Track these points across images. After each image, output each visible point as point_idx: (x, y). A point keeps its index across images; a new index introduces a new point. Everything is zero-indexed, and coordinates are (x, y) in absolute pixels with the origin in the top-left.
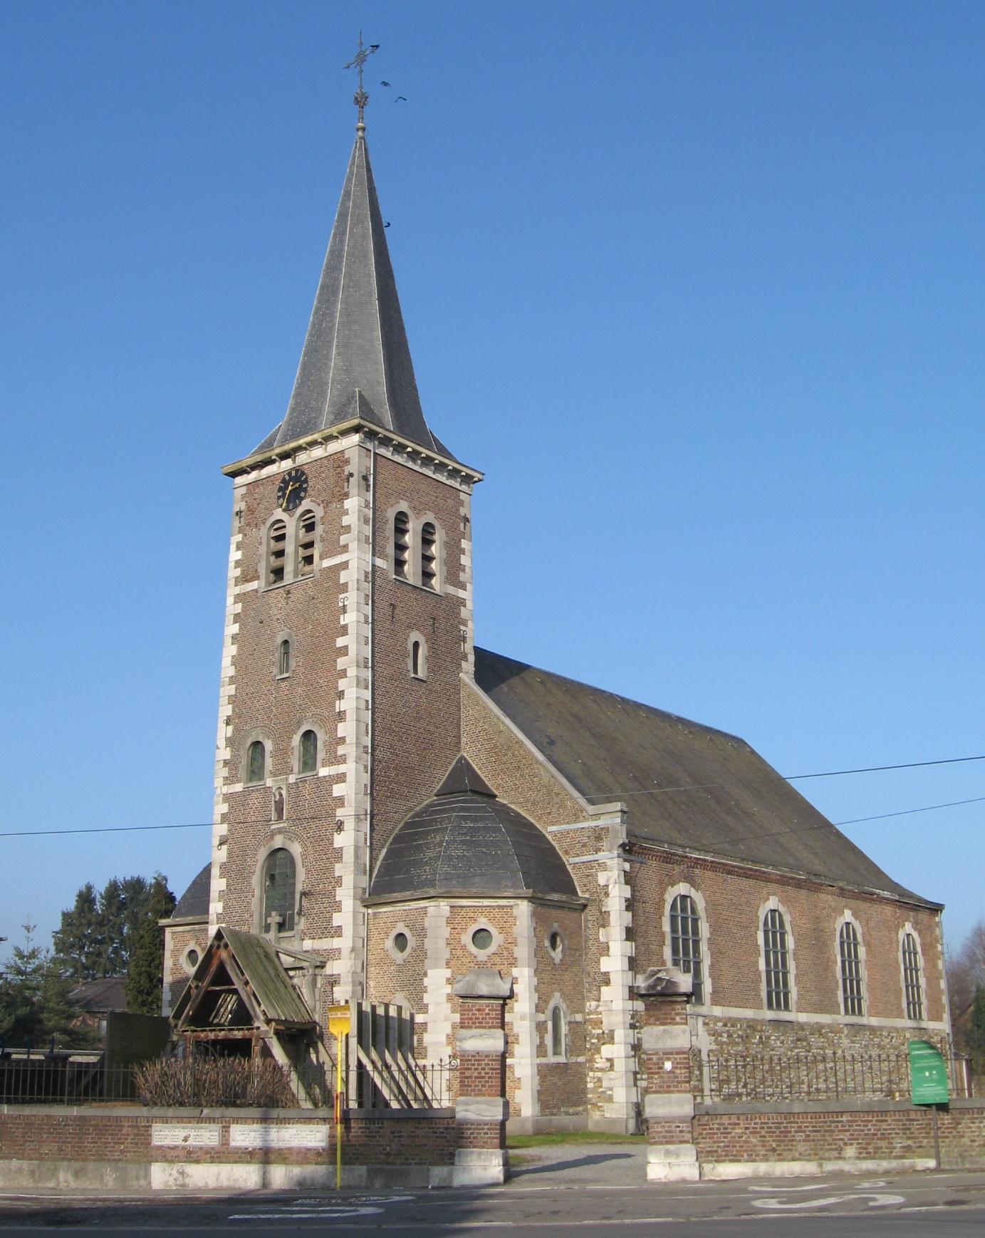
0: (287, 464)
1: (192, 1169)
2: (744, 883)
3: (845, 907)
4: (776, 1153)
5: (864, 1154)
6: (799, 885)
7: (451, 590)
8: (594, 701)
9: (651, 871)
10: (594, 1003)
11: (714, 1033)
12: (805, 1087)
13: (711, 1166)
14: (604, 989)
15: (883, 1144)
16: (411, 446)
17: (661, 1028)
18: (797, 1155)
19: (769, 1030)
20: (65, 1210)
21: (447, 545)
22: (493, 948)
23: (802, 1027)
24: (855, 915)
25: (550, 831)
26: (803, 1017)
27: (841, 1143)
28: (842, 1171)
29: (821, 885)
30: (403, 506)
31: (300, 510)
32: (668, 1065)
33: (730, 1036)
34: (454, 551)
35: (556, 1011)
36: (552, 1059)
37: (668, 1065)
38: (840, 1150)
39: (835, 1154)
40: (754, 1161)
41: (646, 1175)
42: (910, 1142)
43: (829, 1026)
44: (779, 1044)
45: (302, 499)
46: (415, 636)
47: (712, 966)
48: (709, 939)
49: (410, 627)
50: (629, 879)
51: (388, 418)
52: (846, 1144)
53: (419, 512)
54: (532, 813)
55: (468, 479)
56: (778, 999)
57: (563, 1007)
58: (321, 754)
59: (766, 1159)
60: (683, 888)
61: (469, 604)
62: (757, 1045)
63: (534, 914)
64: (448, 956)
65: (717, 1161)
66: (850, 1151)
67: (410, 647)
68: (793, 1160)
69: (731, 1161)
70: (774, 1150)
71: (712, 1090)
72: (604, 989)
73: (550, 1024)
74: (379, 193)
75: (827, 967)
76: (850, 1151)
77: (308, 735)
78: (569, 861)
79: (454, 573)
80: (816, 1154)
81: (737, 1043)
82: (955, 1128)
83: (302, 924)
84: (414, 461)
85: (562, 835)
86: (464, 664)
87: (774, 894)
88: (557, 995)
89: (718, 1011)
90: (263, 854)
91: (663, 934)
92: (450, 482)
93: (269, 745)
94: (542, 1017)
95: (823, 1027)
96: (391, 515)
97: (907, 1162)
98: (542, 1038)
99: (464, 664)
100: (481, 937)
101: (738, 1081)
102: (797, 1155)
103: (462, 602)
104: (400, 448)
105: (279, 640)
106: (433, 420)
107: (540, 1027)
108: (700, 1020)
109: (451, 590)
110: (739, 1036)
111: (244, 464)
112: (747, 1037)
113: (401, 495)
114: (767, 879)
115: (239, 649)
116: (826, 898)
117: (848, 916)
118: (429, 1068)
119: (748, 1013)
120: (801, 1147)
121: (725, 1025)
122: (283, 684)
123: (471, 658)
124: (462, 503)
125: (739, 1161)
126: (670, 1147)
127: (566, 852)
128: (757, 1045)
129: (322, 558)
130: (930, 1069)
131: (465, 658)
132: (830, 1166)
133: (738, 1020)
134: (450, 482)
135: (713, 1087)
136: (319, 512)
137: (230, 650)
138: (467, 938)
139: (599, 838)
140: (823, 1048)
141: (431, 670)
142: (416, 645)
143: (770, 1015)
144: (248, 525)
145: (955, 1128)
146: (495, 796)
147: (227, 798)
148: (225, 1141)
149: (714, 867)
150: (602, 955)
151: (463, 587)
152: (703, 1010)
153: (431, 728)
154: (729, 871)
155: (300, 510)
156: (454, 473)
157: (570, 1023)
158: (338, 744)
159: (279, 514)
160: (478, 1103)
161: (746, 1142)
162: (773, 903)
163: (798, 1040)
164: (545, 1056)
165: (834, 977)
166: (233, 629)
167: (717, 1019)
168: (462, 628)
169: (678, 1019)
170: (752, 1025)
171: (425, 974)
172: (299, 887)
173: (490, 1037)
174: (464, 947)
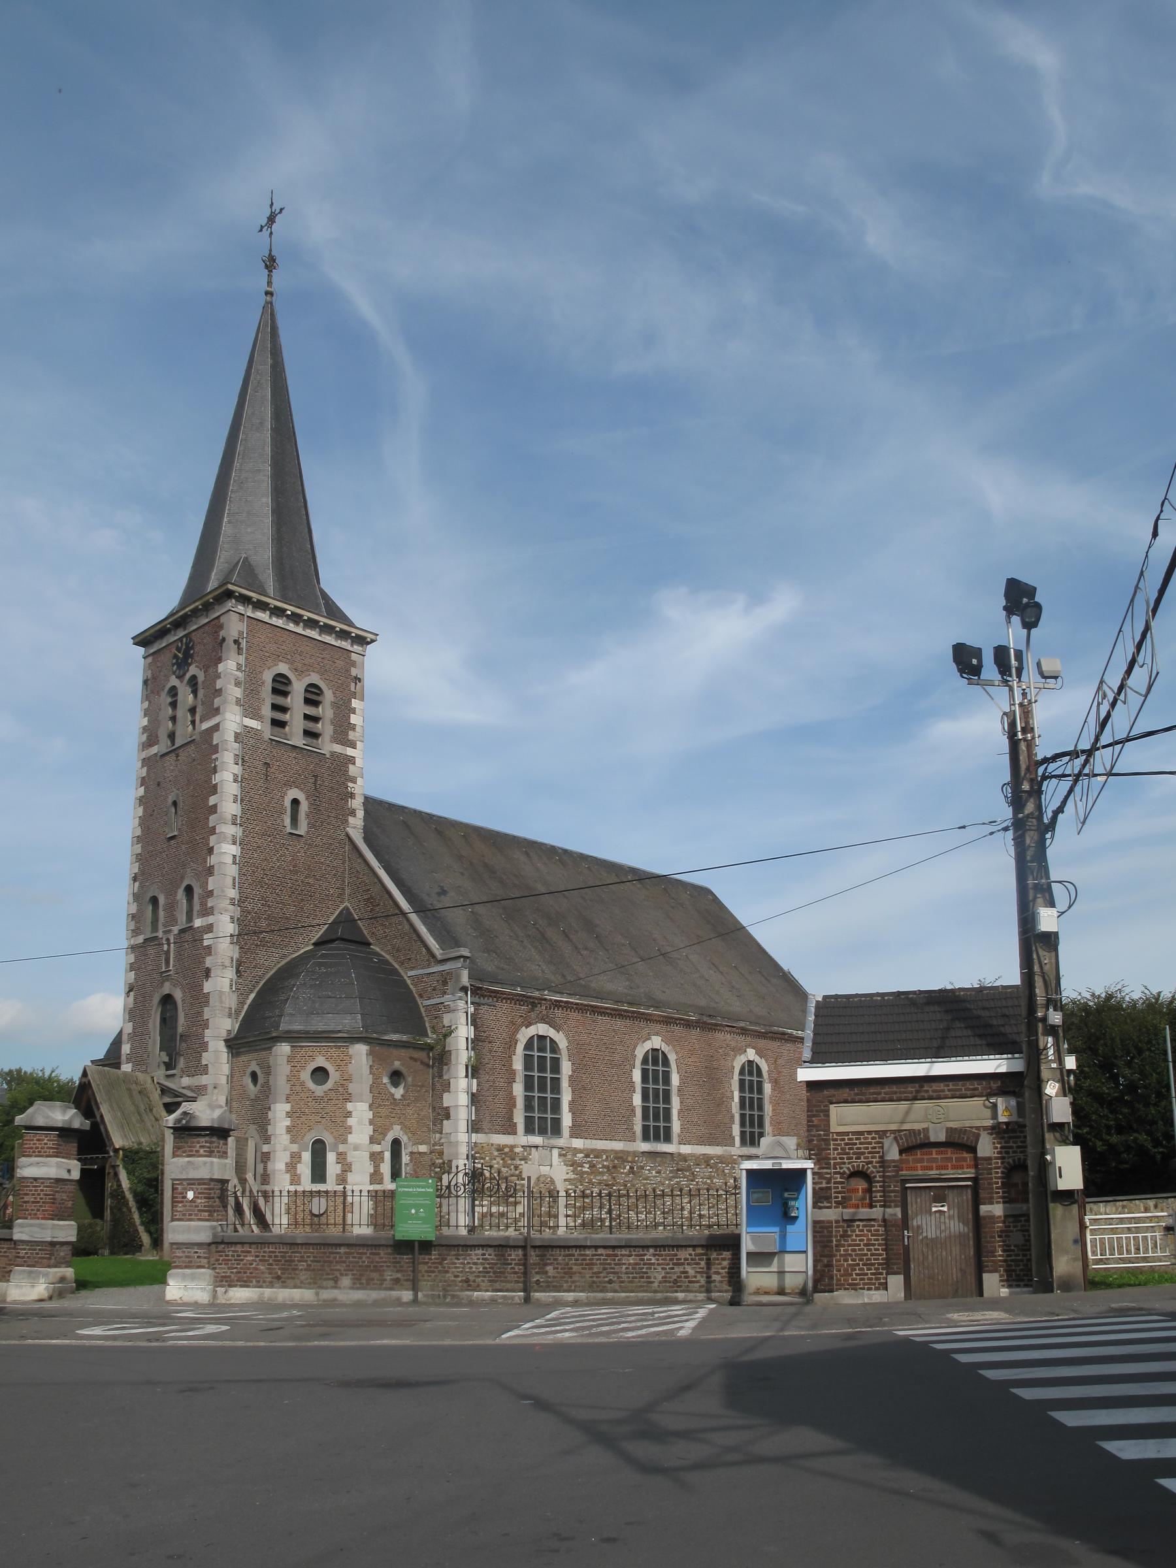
0: (181, 633)
2: (618, 1024)
3: (749, 1046)
4: (279, 1280)
5: (358, 1284)
6: (688, 1024)
7: (338, 748)
8: (527, 854)
9: (499, 1015)
10: (438, 1135)
11: (573, 1164)
12: (686, 1213)
13: (223, 1289)
14: (445, 1122)
15: (375, 1275)
16: (290, 609)
17: (187, 1159)
18: (298, 1282)
19: (643, 1161)
21: (334, 705)
22: (329, 1084)
23: (684, 1158)
24: (759, 1053)
25: (408, 975)
26: (686, 1149)
27: (337, 1274)
28: (335, 1300)
29: (716, 1025)
30: (283, 668)
31: (188, 676)
32: (190, 1195)
33: (592, 1166)
34: (344, 710)
35: (396, 1143)
36: (306, 1184)
37: (190, 1195)
38: (336, 1280)
39: (331, 1283)
40: (261, 1287)
41: (164, 1295)
42: (399, 1275)
43: (719, 1157)
44: (654, 1177)
45: (190, 664)
46: (294, 793)
47: (572, 1103)
48: (570, 1077)
49: (289, 784)
50: (475, 1021)
51: (270, 585)
52: (342, 1275)
53: (300, 673)
54: (396, 958)
55: (362, 641)
56: (657, 1130)
57: (404, 1139)
58: (197, 907)
59: (271, 1285)
60: (542, 1029)
61: (358, 762)
62: (627, 1174)
63: (370, 1053)
64: (288, 1092)
65: (230, 1286)
66: (346, 1281)
67: (287, 803)
68: (295, 1287)
69: (241, 1286)
70: (278, 1278)
71: (567, 1216)
72: (445, 1122)
73: (387, 1155)
75: (721, 1103)
76: (346, 1281)
78: (423, 1003)
79: (343, 731)
80: (315, 1283)
81: (602, 1174)
82: (441, 1263)
83: (182, 1063)
84: (297, 623)
85: (418, 979)
86: (351, 820)
87: (657, 1034)
88: (397, 1128)
89: (578, 1143)
90: (156, 999)
91: (513, 1073)
92: (338, 643)
94: (377, 1148)
95: (712, 1158)
96: (268, 677)
97: (395, 1293)
98: (265, 1169)
99: (351, 820)
100: (320, 1074)
101: (601, 1208)
102: (298, 1282)
103: (352, 760)
104: (278, 612)
105: (170, 801)
106: (331, 581)
107: (376, 1158)
108: (555, 1152)
109: (338, 748)
110: (604, 1167)
111: (1130, 658)
112: (615, 1167)
113: (278, 657)
114: (648, 1018)
115: (145, 811)
116: (724, 1038)
117: (751, 1054)
118: (277, 1193)
119: (618, 1146)
120: (303, 1276)
121: (587, 1156)
122: (173, 842)
123: (360, 814)
124: (354, 664)
125: (248, 1286)
126: (188, 1271)
127: (421, 996)
128: (627, 1174)
129: (201, 722)
131: (353, 813)
132: (326, 1294)
133: (605, 1151)
134: (338, 643)
135: (569, 1213)
136: (201, 677)
138: (306, 1076)
139: (445, 983)
140: (710, 1178)
141: (311, 825)
143: (645, 1147)
144: (152, 692)
145: (441, 1263)
146: (370, 944)
149: (580, 1008)
150: (444, 1091)
151: (353, 745)
152: (561, 1142)
153: (311, 881)
154: (594, 1010)
155: (188, 676)
156: (343, 635)
157: (411, 1153)
158: (208, 897)
159: (174, 681)
160: (31, 1225)
161: (256, 1269)
162: (656, 1042)
163: (678, 1170)
164: (381, 1183)
165: (729, 1111)
167: (576, 1151)
168: (350, 784)
169: (202, 1151)
170: (621, 1156)
171: (269, 1108)
172: (180, 1030)
173: (45, 1164)
174: (302, 1084)
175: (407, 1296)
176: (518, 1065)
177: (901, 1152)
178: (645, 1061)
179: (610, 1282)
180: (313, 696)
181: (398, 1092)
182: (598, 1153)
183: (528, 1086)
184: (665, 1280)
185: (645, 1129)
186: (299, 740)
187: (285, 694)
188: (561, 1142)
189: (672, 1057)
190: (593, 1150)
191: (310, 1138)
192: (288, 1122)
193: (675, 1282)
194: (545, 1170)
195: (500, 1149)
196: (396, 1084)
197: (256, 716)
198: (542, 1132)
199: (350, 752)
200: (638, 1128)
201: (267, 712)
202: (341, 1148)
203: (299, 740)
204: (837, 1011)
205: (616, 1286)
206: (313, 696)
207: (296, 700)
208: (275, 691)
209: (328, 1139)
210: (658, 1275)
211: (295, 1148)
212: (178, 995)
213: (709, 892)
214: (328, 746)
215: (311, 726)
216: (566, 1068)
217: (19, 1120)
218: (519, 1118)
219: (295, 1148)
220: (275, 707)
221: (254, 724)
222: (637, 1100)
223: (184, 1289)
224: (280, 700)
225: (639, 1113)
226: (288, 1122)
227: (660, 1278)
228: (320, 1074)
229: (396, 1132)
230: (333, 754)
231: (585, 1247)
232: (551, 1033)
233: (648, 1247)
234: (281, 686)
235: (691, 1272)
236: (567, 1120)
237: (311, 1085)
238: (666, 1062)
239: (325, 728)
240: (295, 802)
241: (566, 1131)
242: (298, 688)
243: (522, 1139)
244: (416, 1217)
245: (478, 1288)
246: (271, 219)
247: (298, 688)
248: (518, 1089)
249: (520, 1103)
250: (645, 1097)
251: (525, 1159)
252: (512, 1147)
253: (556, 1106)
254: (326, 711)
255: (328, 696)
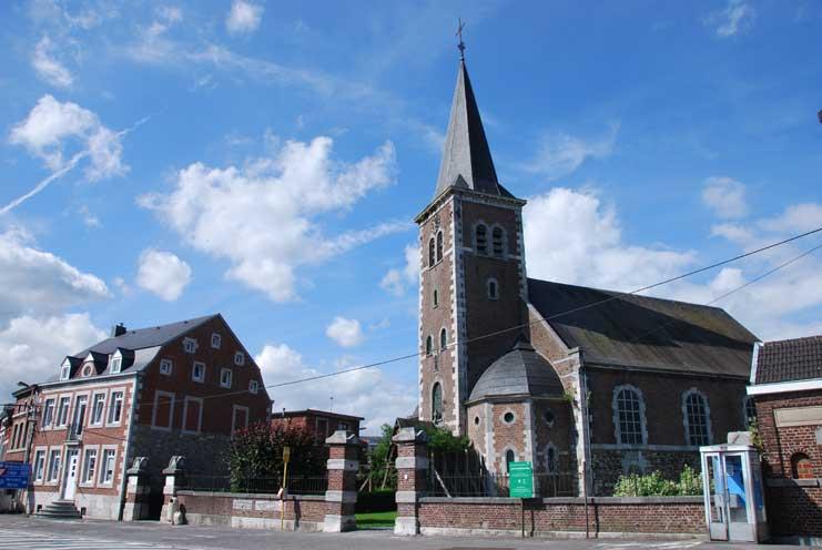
1: (244, 519)
7: (511, 256)
11: (650, 459)
20: (758, 531)
22: (513, 422)
25: (554, 363)
30: (482, 222)
33: (662, 460)
35: (551, 451)
36: (548, 473)
38: (481, 523)
53: (490, 223)
57: (555, 449)
60: (628, 387)
66: (485, 524)
73: (546, 457)
74: (472, 83)
77: (444, 331)
85: (559, 365)
93: (433, 338)
94: (540, 454)
96: (474, 227)
99: (521, 291)
108: (640, 453)
109: (511, 256)
119: (676, 448)
123: (526, 287)
130: (522, 478)
137: (421, 297)
138: (502, 418)
141: (501, 294)
142: (492, 285)
147: (422, 362)
148: (253, 507)
162: (694, 390)
166: (421, 288)
167: (653, 451)
174: (501, 423)
175: (519, 533)
176: (615, 407)
177: (394, 522)
178: (688, 401)
179: (638, 526)
180: (497, 234)
181: (551, 424)
182: (665, 453)
183: (622, 417)
184: (671, 526)
185: (692, 439)
186: (491, 254)
187: (500, 244)
188: (643, 447)
189: (705, 398)
190: (662, 451)
191: (505, 449)
192: (494, 442)
193: (679, 526)
194: (634, 463)
195: (608, 452)
196: (549, 421)
197: (470, 246)
198: (632, 442)
199: (518, 258)
200: (688, 437)
201: (475, 243)
202: (522, 454)
203: (491, 254)
204: (771, 351)
205: (642, 529)
206: (497, 234)
207: (489, 236)
208: (478, 233)
209: (515, 450)
210: (668, 521)
211: (498, 455)
212: (441, 382)
213: (722, 310)
214: (507, 256)
215: (498, 248)
216: (642, 406)
217: (328, 440)
218: (618, 435)
219: (498, 455)
220: (479, 241)
221: (469, 250)
222: (686, 422)
223: (404, 526)
224: (481, 237)
225: (688, 430)
226: (494, 442)
227: (668, 524)
228: (509, 417)
229: (550, 445)
230: (510, 259)
231: (620, 504)
232: (633, 388)
233: (659, 504)
234: (481, 231)
235: (689, 520)
236: (645, 435)
237: (504, 422)
238: (701, 401)
239: (505, 248)
240: (492, 285)
241: (645, 441)
242: (490, 230)
243: (620, 446)
244: (521, 484)
245: (558, 529)
246: (460, 29)
247: (490, 230)
248: (616, 419)
249: (644, 427)
250: (690, 421)
251: (623, 457)
252: (615, 450)
253: (638, 428)
254: (505, 239)
255: (505, 232)
